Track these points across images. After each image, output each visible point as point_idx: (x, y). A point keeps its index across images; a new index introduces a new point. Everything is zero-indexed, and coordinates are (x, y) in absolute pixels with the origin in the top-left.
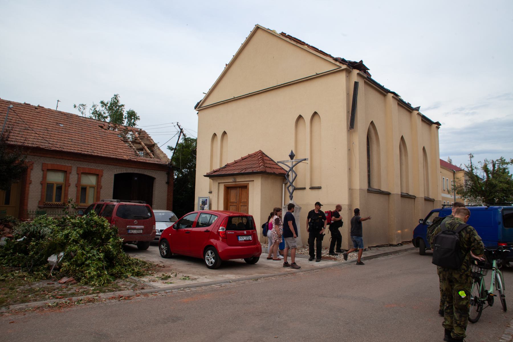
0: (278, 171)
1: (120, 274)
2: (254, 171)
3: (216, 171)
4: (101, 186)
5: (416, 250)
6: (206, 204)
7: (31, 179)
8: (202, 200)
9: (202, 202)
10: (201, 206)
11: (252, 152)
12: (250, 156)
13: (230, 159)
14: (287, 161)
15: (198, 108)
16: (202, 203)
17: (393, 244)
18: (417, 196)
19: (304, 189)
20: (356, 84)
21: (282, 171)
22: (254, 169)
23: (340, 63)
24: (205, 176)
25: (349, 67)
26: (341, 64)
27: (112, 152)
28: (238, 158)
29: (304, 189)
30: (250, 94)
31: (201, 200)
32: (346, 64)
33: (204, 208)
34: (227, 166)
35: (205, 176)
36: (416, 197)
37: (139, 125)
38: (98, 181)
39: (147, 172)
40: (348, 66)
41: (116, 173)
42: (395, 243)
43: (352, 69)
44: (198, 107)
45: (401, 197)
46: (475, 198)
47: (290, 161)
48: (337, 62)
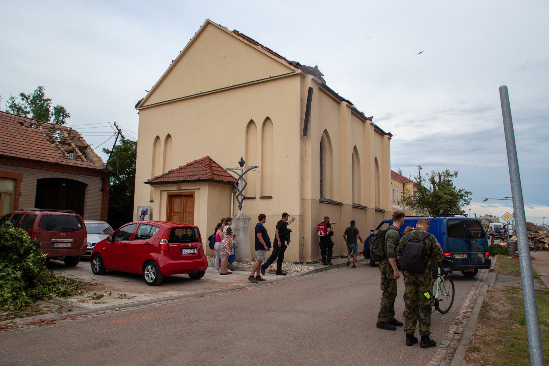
2: (201, 178)
6: (147, 214)
7: (20, 192)
8: (141, 210)
9: (142, 211)
10: (141, 217)
12: (196, 162)
14: (237, 169)
15: (139, 107)
16: (142, 213)
17: (344, 256)
19: (255, 198)
22: (200, 176)
24: (145, 183)
25: (304, 72)
26: (296, 68)
28: (183, 164)
29: (255, 198)
30: (198, 94)
31: (141, 209)
32: (301, 69)
33: (144, 218)
34: (171, 172)
35: (145, 183)
36: (367, 208)
41: (39, 178)
43: (307, 74)
44: (139, 106)
45: (353, 207)
47: (239, 168)
48: (292, 66)
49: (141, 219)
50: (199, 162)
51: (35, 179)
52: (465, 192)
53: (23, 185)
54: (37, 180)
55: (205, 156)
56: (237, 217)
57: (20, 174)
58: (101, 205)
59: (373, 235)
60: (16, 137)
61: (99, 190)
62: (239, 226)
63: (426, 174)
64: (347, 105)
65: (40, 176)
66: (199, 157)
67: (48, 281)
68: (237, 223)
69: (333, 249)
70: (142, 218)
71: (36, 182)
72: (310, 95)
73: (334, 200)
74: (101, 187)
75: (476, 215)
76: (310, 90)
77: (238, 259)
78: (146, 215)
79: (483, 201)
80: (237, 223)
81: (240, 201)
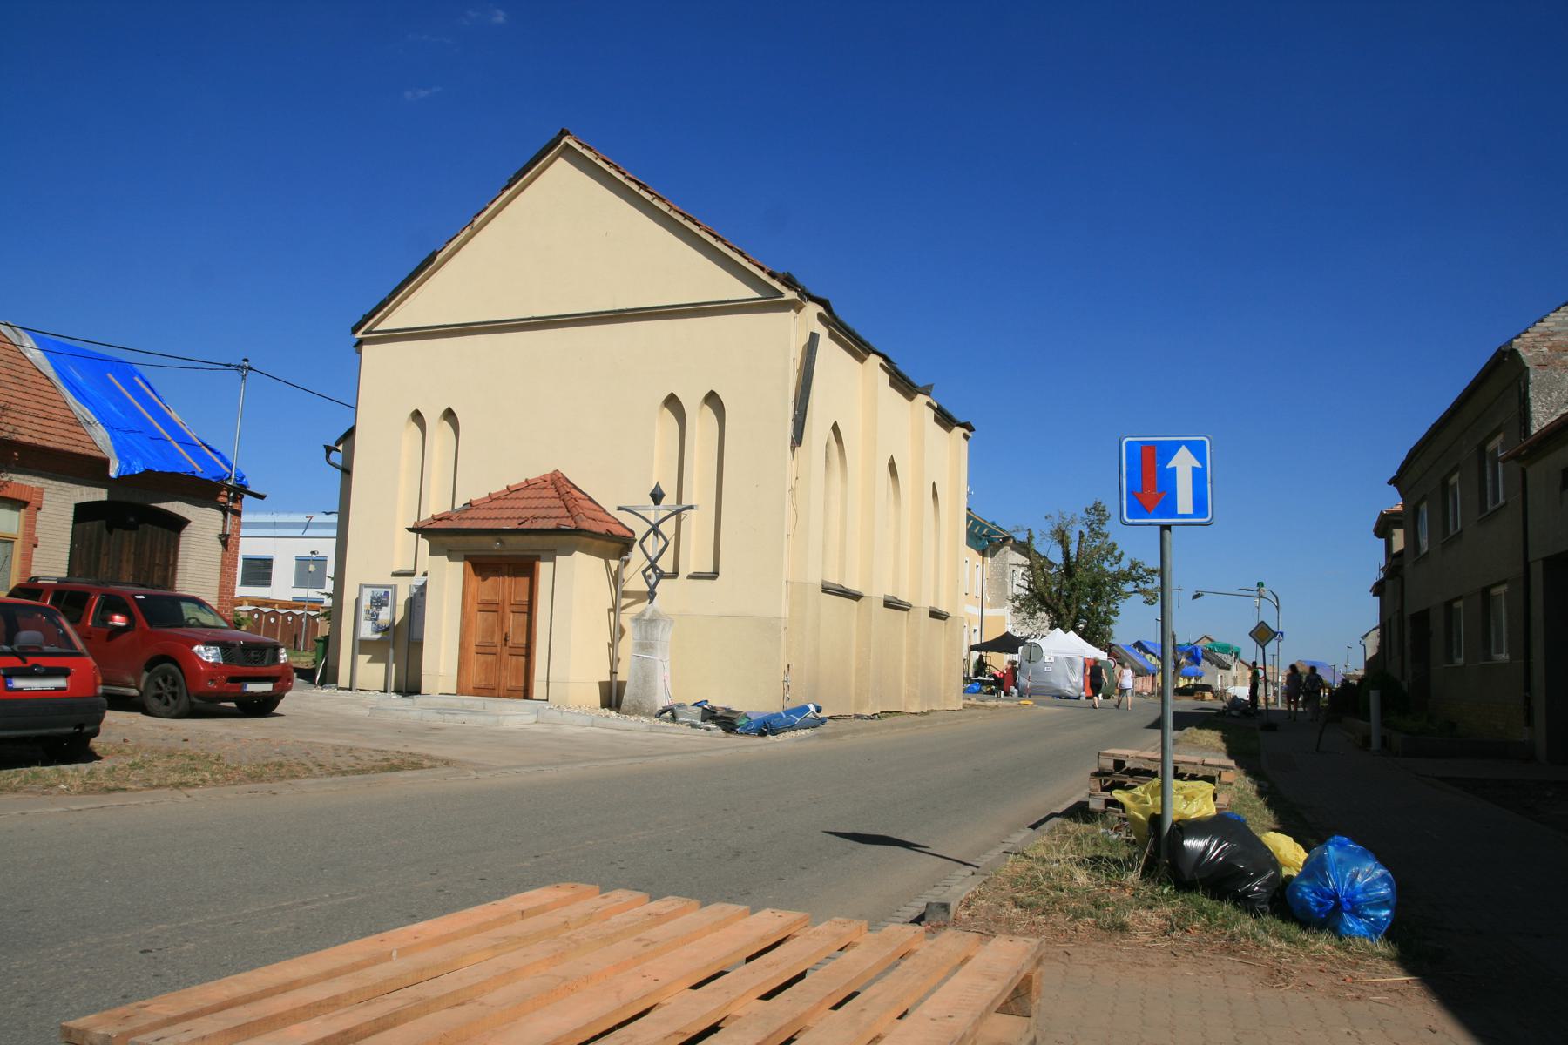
0: (600, 528)
1: (1060, 910)
2: (563, 527)
3: (440, 520)
4: (37, 539)
5: (1138, 751)
6: (386, 605)
7: (36, 535)
8: (370, 595)
9: (373, 598)
11: (516, 480)
12: (528, 485)
13: (475, 488)
14: (645, 508)
15: (363, 333)
16: (372, 603)
17: (862, 716)
18: (914, 605)
20: (814, 337)
21: (624, 532)
23: (783, 283)
25: (801, 297)
27: (66, 434)
28: (498, 487)
32: (796, 290)
33: (378, 615)
34: (470, 505)
35: (409, 529)
36: (911, 606)
37: (1394, 502)
38: (30, 525)
39: (95, 493)
40: (799, 295)
41: (80, 500)
42: (867, 712)
44: (363, 330)
45: (886, 606)
46: (1032, 615)
49: (370, 616)
50: (536, 486)
51: (69, 502)
52: (1145, 570)
53: (42, 519)
54: (73, 507)
55: (549, 471)
56: (645, 618)
57: (37, 488)
58: (219, 578)
59: (1560, 346)
60: (8, 385)
61: (216, 535)
62: (649, 637)
63: (1046, 517)
64: (881, 365)
65: (82, 494)
66: (534, 474)
67: (1154, 585)
68: (646, 632)
69: (1404, 458)
70: (373, 615)
71: (73, 511)
72: (812, 349)
73: (846, 587)
74: (221, 529)
75: (1177, 638)
76: (814, 337)
77: (647, 711)
78: (384, 608)
79: (1191, 597)
80: (646, 632)
81: (652, 581)
